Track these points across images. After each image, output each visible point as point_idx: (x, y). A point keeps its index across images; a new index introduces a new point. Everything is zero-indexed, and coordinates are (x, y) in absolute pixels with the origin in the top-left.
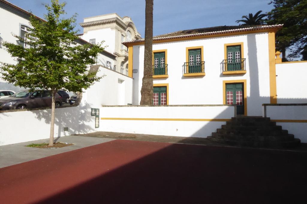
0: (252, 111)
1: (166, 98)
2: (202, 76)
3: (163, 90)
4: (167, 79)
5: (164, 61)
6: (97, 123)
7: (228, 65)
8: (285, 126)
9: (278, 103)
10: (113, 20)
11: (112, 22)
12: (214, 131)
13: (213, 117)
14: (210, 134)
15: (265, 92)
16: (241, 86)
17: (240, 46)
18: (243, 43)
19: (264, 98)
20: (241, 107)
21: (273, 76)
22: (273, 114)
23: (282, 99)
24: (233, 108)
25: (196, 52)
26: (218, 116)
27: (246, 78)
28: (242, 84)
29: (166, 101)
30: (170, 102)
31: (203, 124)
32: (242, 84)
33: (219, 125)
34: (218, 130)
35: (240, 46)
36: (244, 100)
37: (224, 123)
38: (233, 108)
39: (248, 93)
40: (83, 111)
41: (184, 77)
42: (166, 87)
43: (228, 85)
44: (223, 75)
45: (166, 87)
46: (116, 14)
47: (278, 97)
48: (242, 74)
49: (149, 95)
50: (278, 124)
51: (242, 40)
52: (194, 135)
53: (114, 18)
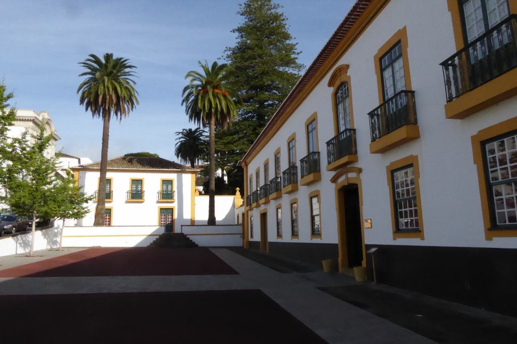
0: (177, 230)
1: (110, 219)
2: (142, 202)
3: (109, 211)
4: (112, 203)
5: (110, 187)
6: (316, 206)
7: (163, 194)
8: (191, 238)
9: (195, 224)
10: (26, 118)
11: (30, 120)
12: (152, 242)
13: (149, 234)
14: (149, 244)
15: (187, 216)
16: (171, 211)
17: (172, 181)
18: (175, 207)
19: (186, 220)
20: (169, 227)
21: (193, 205)
22: (186, 231)
23: (199, 221)
24: (163, 228)
25: (137, 182)
26: (153, 233)
27: (174, 205)
28: (172, 209)
29: (110, 221)
30: (114, 222)
31: (143, 238)
32: (172, 209)
33: (154, 238)
34: (151, 244)
35: (172, 181)
36: (173, 221)
37: (158, 237)
38: (164, 227)
39: (176, 216)
40: (56, 231)
41: (127, 202)
42: (110, 209)
43: (162, 209)
44: (158, 202)
45: (110, 209)
46: (34, 111)
47: (195, 219)
48: (172, 202)
49: (102, 217)
50: (188, 236)
51: (173, 176)
52: (137, 245)
53: (31, 117)
